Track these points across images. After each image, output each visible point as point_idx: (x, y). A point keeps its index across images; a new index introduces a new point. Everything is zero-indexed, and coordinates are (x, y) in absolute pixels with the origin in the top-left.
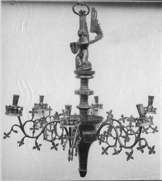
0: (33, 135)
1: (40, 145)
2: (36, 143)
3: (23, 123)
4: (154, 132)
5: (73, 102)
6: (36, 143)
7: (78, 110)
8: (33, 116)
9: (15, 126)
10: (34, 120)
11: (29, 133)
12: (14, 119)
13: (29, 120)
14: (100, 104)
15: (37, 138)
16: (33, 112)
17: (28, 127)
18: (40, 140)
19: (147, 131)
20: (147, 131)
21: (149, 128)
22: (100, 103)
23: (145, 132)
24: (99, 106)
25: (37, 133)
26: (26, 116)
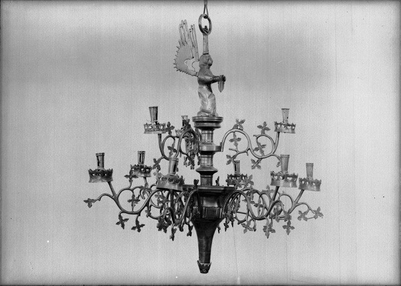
0: (133, 209)
1: (143, 225)
2: (137, 222)
3: (117, 193)
4: (315, 217)
5: (382, 197)
6: (137, 222)
7: (199, 175)
8: (131, 181)
9: (153, 215)
10: (132, 188)
11: (127, 207)
12: (102, 186)
13: (125, 187)
14: (292, 173)
15: (139, 214)
16: (131, 177)
17: (124, 198)
18: (143, 219)
19: (306, 216)
20: (306, 216)
21: (308, 212)
22: (315, 177)
23: (302, 219)
24: (290, 179)
25: (137, 208)
26: (119, 181)
